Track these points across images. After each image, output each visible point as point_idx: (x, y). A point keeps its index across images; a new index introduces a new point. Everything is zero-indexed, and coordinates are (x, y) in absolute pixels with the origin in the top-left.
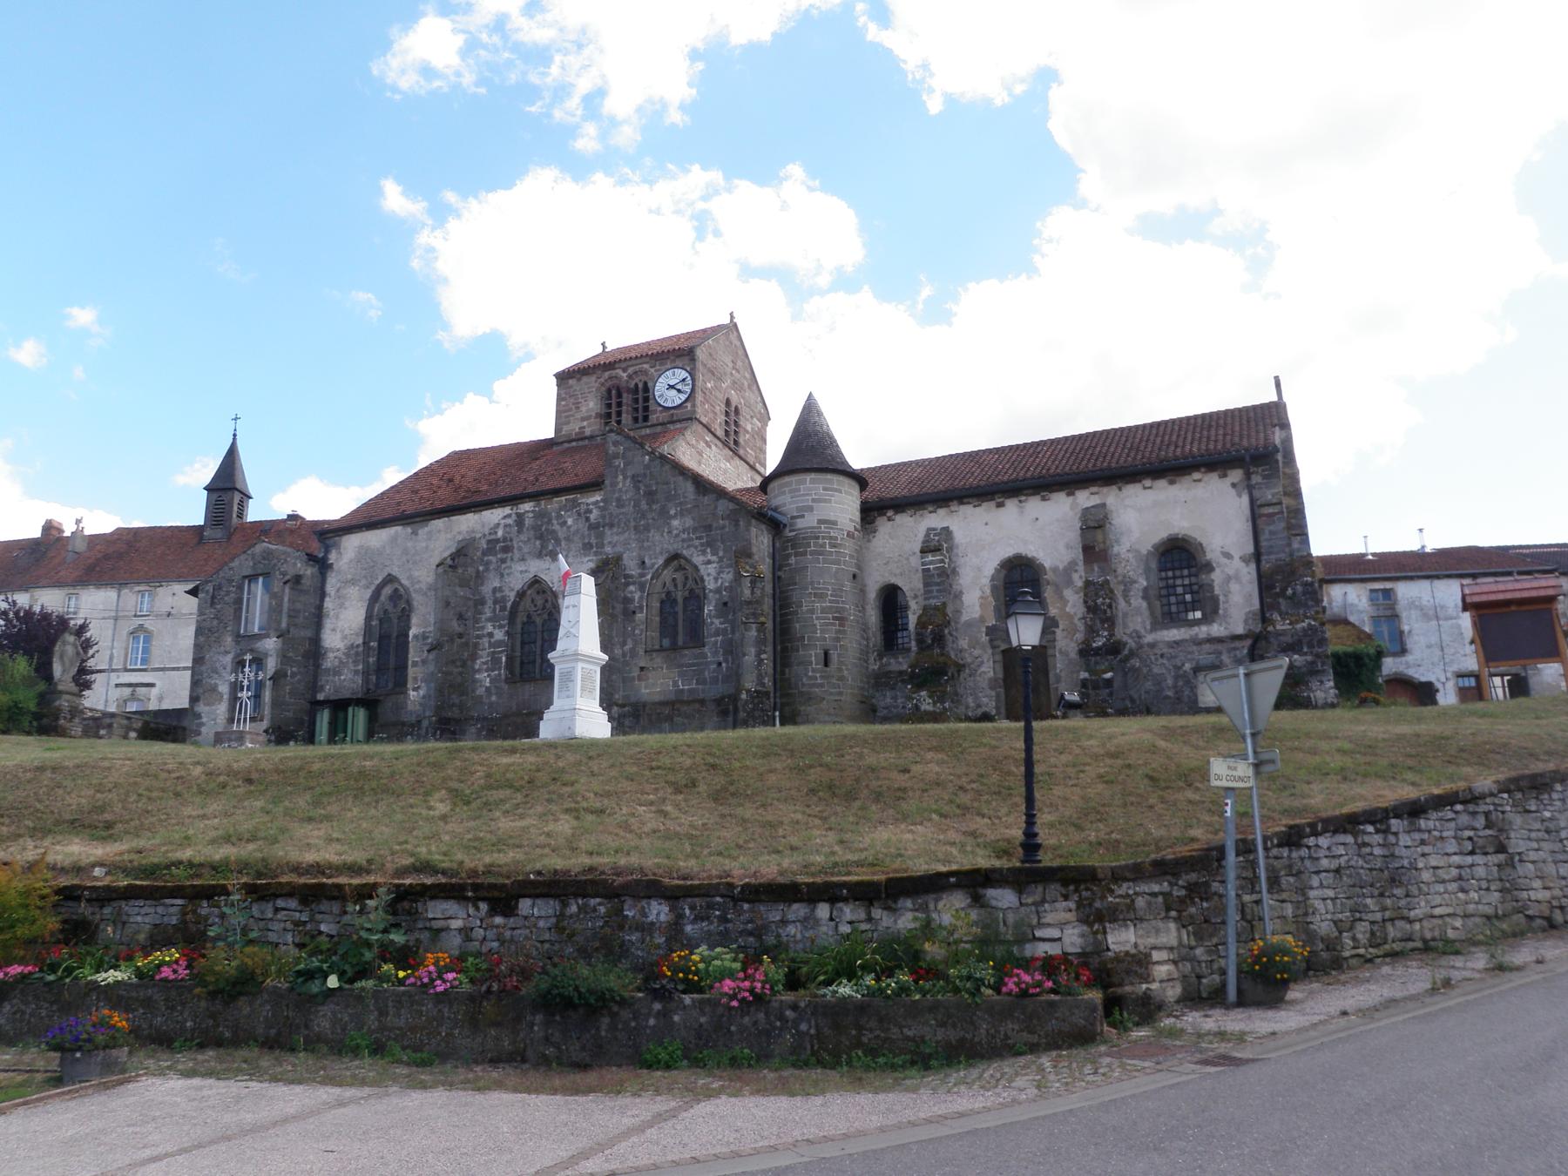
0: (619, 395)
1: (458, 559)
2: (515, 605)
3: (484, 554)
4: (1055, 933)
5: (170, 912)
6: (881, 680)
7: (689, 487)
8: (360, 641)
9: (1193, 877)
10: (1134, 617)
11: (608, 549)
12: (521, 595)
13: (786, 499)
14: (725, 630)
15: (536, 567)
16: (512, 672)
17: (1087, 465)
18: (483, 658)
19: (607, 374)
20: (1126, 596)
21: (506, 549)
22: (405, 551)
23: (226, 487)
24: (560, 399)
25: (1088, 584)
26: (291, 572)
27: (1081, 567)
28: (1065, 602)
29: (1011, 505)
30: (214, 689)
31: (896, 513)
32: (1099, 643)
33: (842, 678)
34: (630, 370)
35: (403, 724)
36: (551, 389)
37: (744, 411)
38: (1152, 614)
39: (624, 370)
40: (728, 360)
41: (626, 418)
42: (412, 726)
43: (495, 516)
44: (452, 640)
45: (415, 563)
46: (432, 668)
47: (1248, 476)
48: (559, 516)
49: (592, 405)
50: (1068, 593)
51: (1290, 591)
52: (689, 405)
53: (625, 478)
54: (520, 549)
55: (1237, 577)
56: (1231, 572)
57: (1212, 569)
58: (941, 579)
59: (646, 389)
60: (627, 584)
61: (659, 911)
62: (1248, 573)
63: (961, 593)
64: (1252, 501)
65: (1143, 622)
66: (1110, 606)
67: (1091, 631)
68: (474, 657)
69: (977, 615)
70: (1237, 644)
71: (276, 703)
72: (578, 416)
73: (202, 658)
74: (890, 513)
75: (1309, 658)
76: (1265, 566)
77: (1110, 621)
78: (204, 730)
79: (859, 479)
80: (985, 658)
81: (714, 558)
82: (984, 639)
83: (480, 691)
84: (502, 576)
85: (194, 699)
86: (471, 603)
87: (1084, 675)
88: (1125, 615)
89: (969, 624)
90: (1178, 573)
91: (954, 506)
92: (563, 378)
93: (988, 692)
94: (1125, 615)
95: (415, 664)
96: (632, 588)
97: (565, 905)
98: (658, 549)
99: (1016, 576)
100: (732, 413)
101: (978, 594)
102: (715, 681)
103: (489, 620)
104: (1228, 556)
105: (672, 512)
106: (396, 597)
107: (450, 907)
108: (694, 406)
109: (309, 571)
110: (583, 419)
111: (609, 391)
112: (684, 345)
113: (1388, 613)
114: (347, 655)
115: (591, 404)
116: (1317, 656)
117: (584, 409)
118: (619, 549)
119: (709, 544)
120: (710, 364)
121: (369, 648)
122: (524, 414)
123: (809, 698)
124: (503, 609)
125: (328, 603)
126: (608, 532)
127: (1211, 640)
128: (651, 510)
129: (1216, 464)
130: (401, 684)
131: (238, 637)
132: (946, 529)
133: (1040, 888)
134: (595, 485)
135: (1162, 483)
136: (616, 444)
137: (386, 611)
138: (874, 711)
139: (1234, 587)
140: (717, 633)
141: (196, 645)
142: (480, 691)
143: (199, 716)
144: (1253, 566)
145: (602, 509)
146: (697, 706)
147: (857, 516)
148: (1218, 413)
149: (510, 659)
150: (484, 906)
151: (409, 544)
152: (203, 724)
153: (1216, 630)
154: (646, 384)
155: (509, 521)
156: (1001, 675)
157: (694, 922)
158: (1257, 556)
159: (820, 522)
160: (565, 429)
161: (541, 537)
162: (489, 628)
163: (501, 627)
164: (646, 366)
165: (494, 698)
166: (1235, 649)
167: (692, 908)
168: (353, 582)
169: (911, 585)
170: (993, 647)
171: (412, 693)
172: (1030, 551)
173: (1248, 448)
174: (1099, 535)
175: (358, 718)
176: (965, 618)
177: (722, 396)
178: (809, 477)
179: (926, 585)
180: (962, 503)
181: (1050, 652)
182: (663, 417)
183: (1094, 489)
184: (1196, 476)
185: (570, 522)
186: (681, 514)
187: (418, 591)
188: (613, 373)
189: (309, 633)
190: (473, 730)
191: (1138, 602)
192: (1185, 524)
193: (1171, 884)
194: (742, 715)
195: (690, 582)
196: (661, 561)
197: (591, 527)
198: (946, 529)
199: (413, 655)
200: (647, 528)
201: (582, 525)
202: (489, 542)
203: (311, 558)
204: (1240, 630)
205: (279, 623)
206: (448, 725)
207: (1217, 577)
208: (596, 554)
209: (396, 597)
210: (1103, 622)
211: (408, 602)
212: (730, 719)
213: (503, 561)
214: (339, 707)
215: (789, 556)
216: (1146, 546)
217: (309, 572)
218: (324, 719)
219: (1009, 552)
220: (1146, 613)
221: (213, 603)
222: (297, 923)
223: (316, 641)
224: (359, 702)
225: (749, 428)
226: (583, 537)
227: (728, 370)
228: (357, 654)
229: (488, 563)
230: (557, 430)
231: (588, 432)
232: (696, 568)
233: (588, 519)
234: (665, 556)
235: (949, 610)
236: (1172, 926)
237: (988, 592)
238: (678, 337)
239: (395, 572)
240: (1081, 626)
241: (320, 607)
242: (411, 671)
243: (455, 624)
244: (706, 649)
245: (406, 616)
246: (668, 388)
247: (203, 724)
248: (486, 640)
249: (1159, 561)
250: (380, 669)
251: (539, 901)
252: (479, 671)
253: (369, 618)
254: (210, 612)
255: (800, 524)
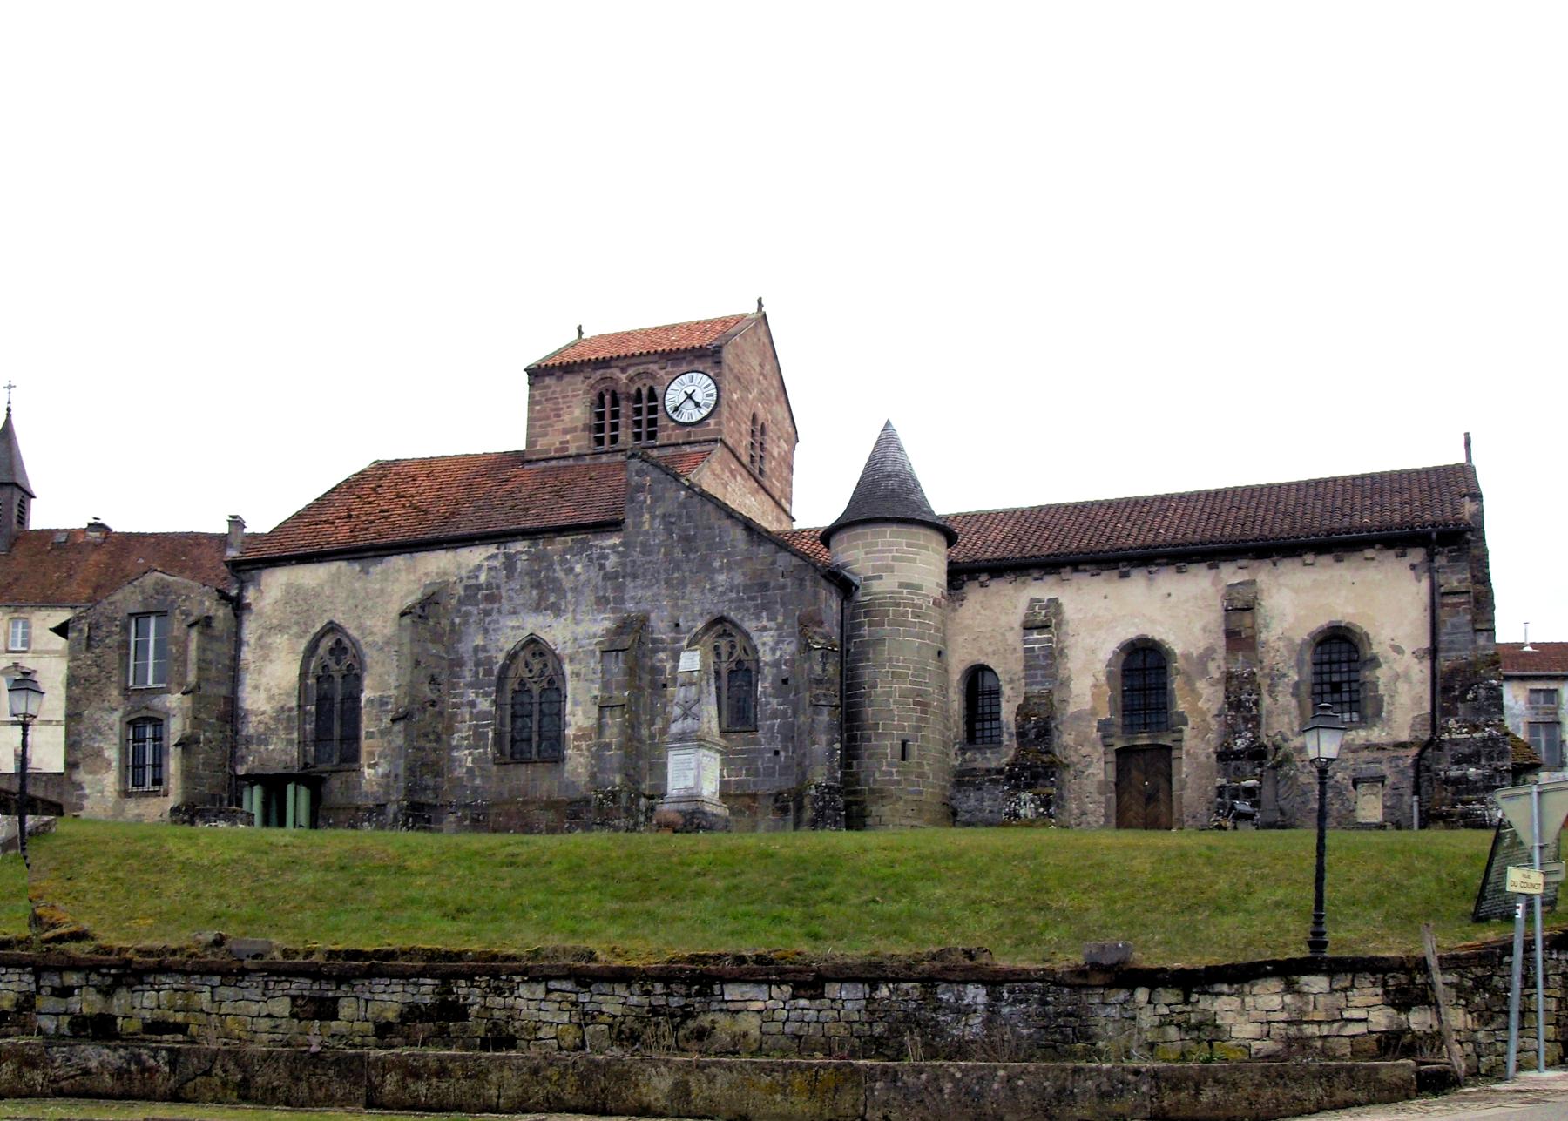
0: (615, 402)
1: (424, 609)
2: (505, 668)
3: (461, 602)
4: (1361, 1014)
5: (426, 990)
6: (964, 779)
7: (739, 534)
8: (294, 703)
9: (1479, 972)
10: (1281, 714)
11: (630, 606)
12: (512, 656)
13: (855, 555)
14: (785, 712)
15: (533, 623)
16: (502, 752)
17: (1233, 533)
18: (463, 731)
19: (598, 374)
20: (1271, 693)
21: (491, 598)
22: (352, 593)
23: (236, 522)
24: (532, 402)
25: (1229, 677)
26: (196, 614)
27: (1221, 652)
28: (1197, 696)
29: (1138, 578)
30: (98, 753)
31: (992, 578)
32: (1240, 744)
33: (921, 775)
34: (631, 371)
35: (358, 809)
36: (520, 386)
37: (772, 431)
38: (1302, 714)
39: (623, 370)
40: (755, 362)
41: (625, 435)
42: (370, 811)
43: (475, 556)
44: (424, 710)
45: (365, 609)
46: (399, 741)
47: (1431, 557)
48: (563, 561)
49: (578, 412)
50: (1201, 685)
51: (1470, 695)
52: (712, 421)
53: (653, 517)
54: (510, 599)
55: (1407, 676)
56: (1399, 668)
57: (1379, 665)
58: (1045, 663)
59: (652, 396)
60: (656, 651)
61: (976, 995)
62: (1420, 672)
63: (1069, 678)
64: (1434, 588)
65: (1290, 723)
66: (1256, 703)
67: (1232, 731)
68: (450, 730)
69: (1087, 707)
70: (1402, 752)
71: (188, 775)
72: (560, 426)
73: (80, 715)
74: (984, 577)
75: (1488, 772)
76: (1444, 664)
77: (1256, 720)
78: (86, 803)
79: (947, 531)
80: (1096, 756)
81: (771, 624)
82: (1095, 735)
83: (460, 772)
84: (486, 631)
85: (71, 765)
86: (444, 663)
87: (1222, 781)
88: (1270, 713)
89: (1078, 717)
90: (1335, 667)
91: (1066, 573)
92: (537, 374)
93: (1097, 797)
94: (1270, 713)
95: (370, 735)
96: (662, 655)
97: (874, 989)
98: (697, 609)
99: (1138, 663)
100: (758, 430)
101: (1090, 681)
102: (770, 772)
103: (470, 685)
104: (1398, 650)
105: (717, 564)
106: (339, 650)
107: (748, 990)
108: (719, 423)
109: (221, 612)
110: (565, 431)
111: (601, 396)
112: (705, 341)
113: (1549, 719)
114: (276, 720)
115: (577, 412)
116: (1496, 770)
117: (566, 418)
118: (644, 606)
119: (764, 607)
120: (737, 368)
121: (306, 713)
122: (488, 418)
123: (881, 795)
124: (489, 672)
125: (247, 654)
126: (629, 583)
127: (1368, 747)
128: (688, 560)
129: (1395, 540)
130: (351, 756)
131: (126, 691)
132: (1054, 601)
133: (1350, 976)
134: (614, 526)
135: (1326, 559)
136: (639, 473)
137: (325, 667)
138: (955, 814)
139: (1402, 686)
140: (774, 715)
141: (69, 698)
142: (460, 772)
143: (79, 786)
144: (1427, 663)
145: (622, 555)
146: (748, 801)
147: (943, 579)
148: (1391, 474)
149: (499, 736)
150: (787, 989)
151: (357, 585)
152: (85, 796)
153: (1377, 735)
154: (651, 390)
155: (496, 563)
156: (1112, 778)
157: (1013, 1004)
158: (1433, 652)
159: (901, 585)
160: (542, 443)
161: (538, 585)
162: (472, 697)
163: (486, 695)
164: (653, 367)
165: (478, 782)
166: (1398, 758)
167: (1011, 992)
168: (280, 628)
169: (1008, 669)
170: (1106, 746)
171: (367, 771)
172: (1157, 632)
173: (1430, 523)
174: (1247, 619)
175: (297, 800)
176: (1072, 709)
177: (748, 411)
178: (889, 530)
179: (1027, 667)
180: (1076, 570)
181: (1174, 753)
182: (678, 436)
183: (1244, 563)
184: (1369, 553)
185: (578, 568)
186: (729, 568)
187: (373, 645)
188: (608, 373)
189: (224, 691)
190: (452, 818)
191: (1286, 699)
192: (1350, 610)
193: (1462, 976)
194: (809, 814)
195: (738, 652)
196: (700, 625)
197: (606, 577)
198: (1054, 601)
199: (367, 724)
200: (682, 583)
201: (595, 575)
202: (467, 588)
203: (223, 596)
204: (1405, 736)
205: (184, 675)
206: (419, 814)
207: (1382, 675)
208: (614, 611)
209: (339, 650)
210: (1246, 721)
211: (359, 657)
212: (791, 817)
213: (487, 613)
214: (274, 786)
215: (861, 625)
216: (1302, 634)
217: (221, 613)
218: (254, 799)
219: (1131, 633)
220: (1295, 713)
221: (89, 647)
222: (574, 1004)
223: (232, 701)
224: (298, 779)
225: (775, 452)
226: (596, 588)
227: (755, 376)
228: (289, 719)
229: (468, 614)
230: (530, 442)
231: (573, 451)
232: (747, 636)
233: (602, 567)
234: (707, 618)
235: (1056, 698)
236: (1461, 1011)
237: (1103, 679)
238: (690, 328)
239: (339, 619)
240: (1214, 724)
241: (236, 658)
242: (365, 744)
243: (426, 688)
244: (759, 734)
245: (354, 679)
246: (687, 395)
247: (85, 796)
248: (466, 710)
249: (1315, 652)
250: (322, 736)
251: (846, 985)
252: (458, 748)
253: (303, 675)
254: (86, 658)
255: (877, 586)
